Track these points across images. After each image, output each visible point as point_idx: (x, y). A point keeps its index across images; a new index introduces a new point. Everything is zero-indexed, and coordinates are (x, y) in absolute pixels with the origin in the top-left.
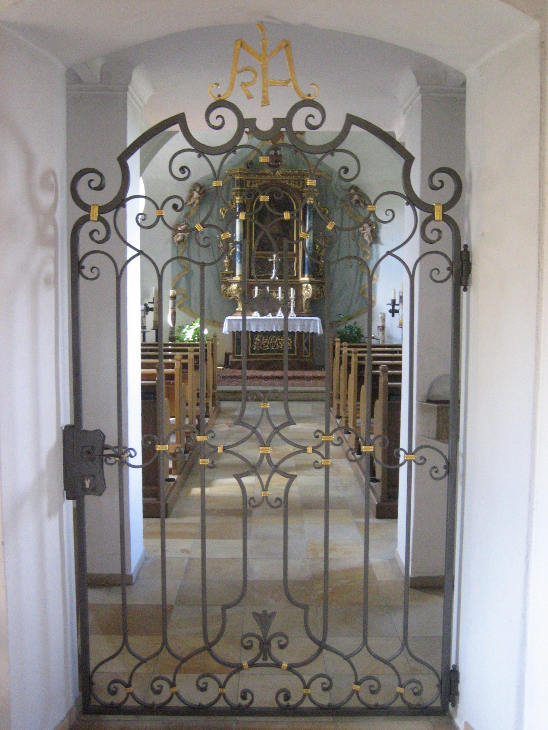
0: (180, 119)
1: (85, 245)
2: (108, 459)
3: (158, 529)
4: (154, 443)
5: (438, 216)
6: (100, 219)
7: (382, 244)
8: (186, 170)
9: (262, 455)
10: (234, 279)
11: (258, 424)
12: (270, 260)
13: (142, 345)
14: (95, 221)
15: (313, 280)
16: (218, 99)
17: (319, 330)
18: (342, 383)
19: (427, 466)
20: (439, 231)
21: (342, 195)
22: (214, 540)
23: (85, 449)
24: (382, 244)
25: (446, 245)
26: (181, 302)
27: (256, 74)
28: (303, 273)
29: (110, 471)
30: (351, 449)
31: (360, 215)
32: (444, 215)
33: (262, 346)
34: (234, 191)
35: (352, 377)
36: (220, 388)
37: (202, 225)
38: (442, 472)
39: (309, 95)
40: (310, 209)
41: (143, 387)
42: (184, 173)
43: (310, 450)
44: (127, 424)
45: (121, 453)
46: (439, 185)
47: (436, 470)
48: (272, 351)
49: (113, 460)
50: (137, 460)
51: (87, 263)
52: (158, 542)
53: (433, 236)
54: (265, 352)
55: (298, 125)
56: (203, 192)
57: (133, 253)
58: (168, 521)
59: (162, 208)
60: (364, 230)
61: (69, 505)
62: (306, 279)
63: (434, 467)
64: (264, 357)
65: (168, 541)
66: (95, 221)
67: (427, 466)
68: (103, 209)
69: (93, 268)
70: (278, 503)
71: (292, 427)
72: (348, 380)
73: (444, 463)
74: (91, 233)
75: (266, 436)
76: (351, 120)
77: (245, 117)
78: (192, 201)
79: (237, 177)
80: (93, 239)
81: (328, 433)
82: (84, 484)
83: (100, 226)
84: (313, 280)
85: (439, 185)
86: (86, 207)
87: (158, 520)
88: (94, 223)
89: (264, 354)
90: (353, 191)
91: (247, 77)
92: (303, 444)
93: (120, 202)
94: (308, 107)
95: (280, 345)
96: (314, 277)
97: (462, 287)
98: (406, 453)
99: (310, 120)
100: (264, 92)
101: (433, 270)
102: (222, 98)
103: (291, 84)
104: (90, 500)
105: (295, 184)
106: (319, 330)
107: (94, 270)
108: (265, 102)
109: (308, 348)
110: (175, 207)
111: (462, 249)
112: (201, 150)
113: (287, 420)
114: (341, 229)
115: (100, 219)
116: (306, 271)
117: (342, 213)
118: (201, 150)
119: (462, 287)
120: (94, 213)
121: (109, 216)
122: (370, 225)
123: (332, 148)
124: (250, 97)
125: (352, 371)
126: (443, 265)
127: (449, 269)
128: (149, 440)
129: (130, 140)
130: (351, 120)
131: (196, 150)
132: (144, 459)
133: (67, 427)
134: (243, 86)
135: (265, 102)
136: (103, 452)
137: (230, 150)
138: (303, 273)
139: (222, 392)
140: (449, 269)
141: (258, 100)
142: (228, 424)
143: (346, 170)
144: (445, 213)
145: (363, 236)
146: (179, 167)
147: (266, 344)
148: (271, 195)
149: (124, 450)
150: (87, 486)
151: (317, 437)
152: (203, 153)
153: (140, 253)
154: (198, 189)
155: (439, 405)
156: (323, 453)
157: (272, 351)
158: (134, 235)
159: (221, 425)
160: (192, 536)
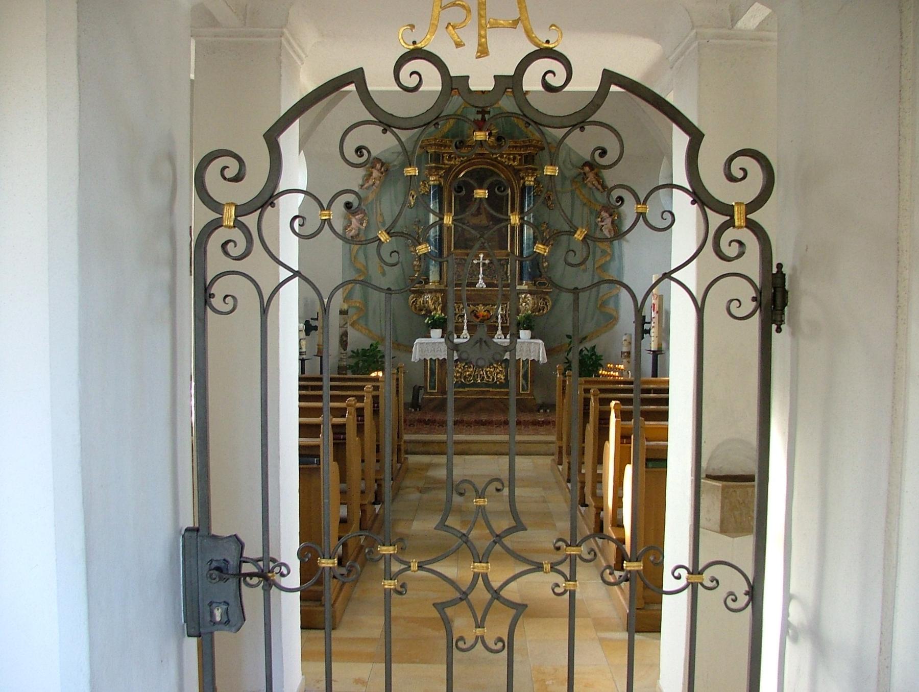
0: (357, 77)
1: (216, 262)
2: (248, 579)
3: (321, 647)
4: (316, 556)
5: (739, 220)
6: (238, 224)
7: (627, 241)
8: (364, 151)
9: (476, 576)
10: (427, 287)
11: (490, 603)
12: (475, 262)
13: (300, 379)
14: (229, 227)
15: (534, 288)
16: (412, 47)
17: (542, 358)
18: (576, 434)
19: (721, 592)
20: (741, 244)
21: (574, 172)
22: (400, 665)
23: (215, 564)
24: (627, 241)
25: (751, 264)
26: (355, 318)
27: (469, 11)
28: (521, 279)
29: (252, 596)
30: (609, 567)
31: (596, 200)
32: (747, 220)
33: (465, 378)
34: (427, 168)
35: (590, 428)
36: (406, 437)
37: (388, 233)
38: (743, 599)
39: (548, 42)
40: (529, 193)
41: (301, 447)
42: (361, 156)
43: (547, 567)
44: (278, 507)
45: (267, 575)
46: (740, 174)
47: (733, 597)
48: (478, 385)
49: (255, 580)
50: (294, 580)
51: (218, 290)
52: (322, 667)
53: (732, 251)
54: (469, 386)
55: (531, 82)
56: (387, 170)
57: (286, 274)
58: (335, 634)
59: (329, 208)
60: (602, 221)
61: (192, 644)
62: (524, 287)
63: (731, 594)
64: (467, 393)
65: (334, 666)
66: (229, 227)
67: (721, 592)
68: (242, 210)
69: (226, 296)
70: (500, 645)
71: (521, 533)
72: (584, 435)
73: (746, 588)
74: (224, 245)
75: (482, 545)
76: (609, 77)
77: (452, 74)
78: (371, 182)
79: (431, 150)
80: (226, 253)
81: (574, 543)
82: (212, 614)
83: (237, 235)
84: (534, 288)
85: (740, 174)
86: (216, 206)
87: (321, 634)
88: (227, 229)
89: (466, 389)
90: (587, 169)
91: (456, 15)
92: (536, 558)
93: (268, 199)
94: (546, 59)
95: (488, 377)
96: (535, 285)
97: (774, 327)
98: (689, 573)
99: (549, 78)
100: (480, 36)
101: (732, 300)
102: (419, 45)
103: (520, 25)
104: (221, 637)
105: (509, 159)
106: (542, 358)
107: (229, 299)
108: (483, 51)
109: (526, 380)
110: (348, 205)
111: (775, 270)
112: (387, 122)
113: (513, 524)
114: (595, 240)
115: (238, 224)
116: (526, 276)
117: (573, 198)
118: (387, 122)
119: (774, 327)
120: (229, 214)
121: (250, 221)
122: (611, 215)
123: (581, 120)
124: (459, 45)
125: (591, 418)
126: (747, 293)
127: (754, 299)
128: (309, 552)
129: (287, 104)
130: (609, 77)
131: (380, 123)
132: (303, 581)
133: (187, 530)
134: (450, 28)
135: (483, 51)
136: (240, 567)
137: (429, 123)
138: (521, 279)
139: (410, 442)
140: (754, 299)
141: (472, 47)
142: (418, 488)
143: (604, 153)
144: (748, 216)
145: (601, 230)
146: (355, 147)
147: (470, 375)
148: (490, 189)
149: (271, 565)
150: (218, 619)
151: (558, 549)
152: (390, 126)
153: (296, 274)
154: (378, 166)
155: (725, 483)
156: (567, 572)
157: (478, 385)
158: (290, 249)
159: (408, 490)
160: (370, 658)
